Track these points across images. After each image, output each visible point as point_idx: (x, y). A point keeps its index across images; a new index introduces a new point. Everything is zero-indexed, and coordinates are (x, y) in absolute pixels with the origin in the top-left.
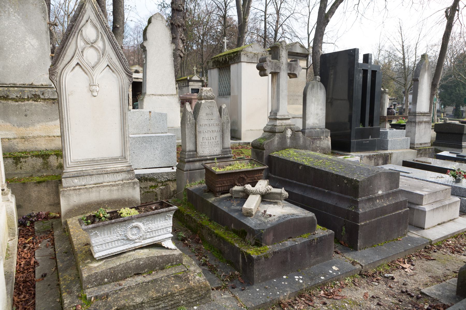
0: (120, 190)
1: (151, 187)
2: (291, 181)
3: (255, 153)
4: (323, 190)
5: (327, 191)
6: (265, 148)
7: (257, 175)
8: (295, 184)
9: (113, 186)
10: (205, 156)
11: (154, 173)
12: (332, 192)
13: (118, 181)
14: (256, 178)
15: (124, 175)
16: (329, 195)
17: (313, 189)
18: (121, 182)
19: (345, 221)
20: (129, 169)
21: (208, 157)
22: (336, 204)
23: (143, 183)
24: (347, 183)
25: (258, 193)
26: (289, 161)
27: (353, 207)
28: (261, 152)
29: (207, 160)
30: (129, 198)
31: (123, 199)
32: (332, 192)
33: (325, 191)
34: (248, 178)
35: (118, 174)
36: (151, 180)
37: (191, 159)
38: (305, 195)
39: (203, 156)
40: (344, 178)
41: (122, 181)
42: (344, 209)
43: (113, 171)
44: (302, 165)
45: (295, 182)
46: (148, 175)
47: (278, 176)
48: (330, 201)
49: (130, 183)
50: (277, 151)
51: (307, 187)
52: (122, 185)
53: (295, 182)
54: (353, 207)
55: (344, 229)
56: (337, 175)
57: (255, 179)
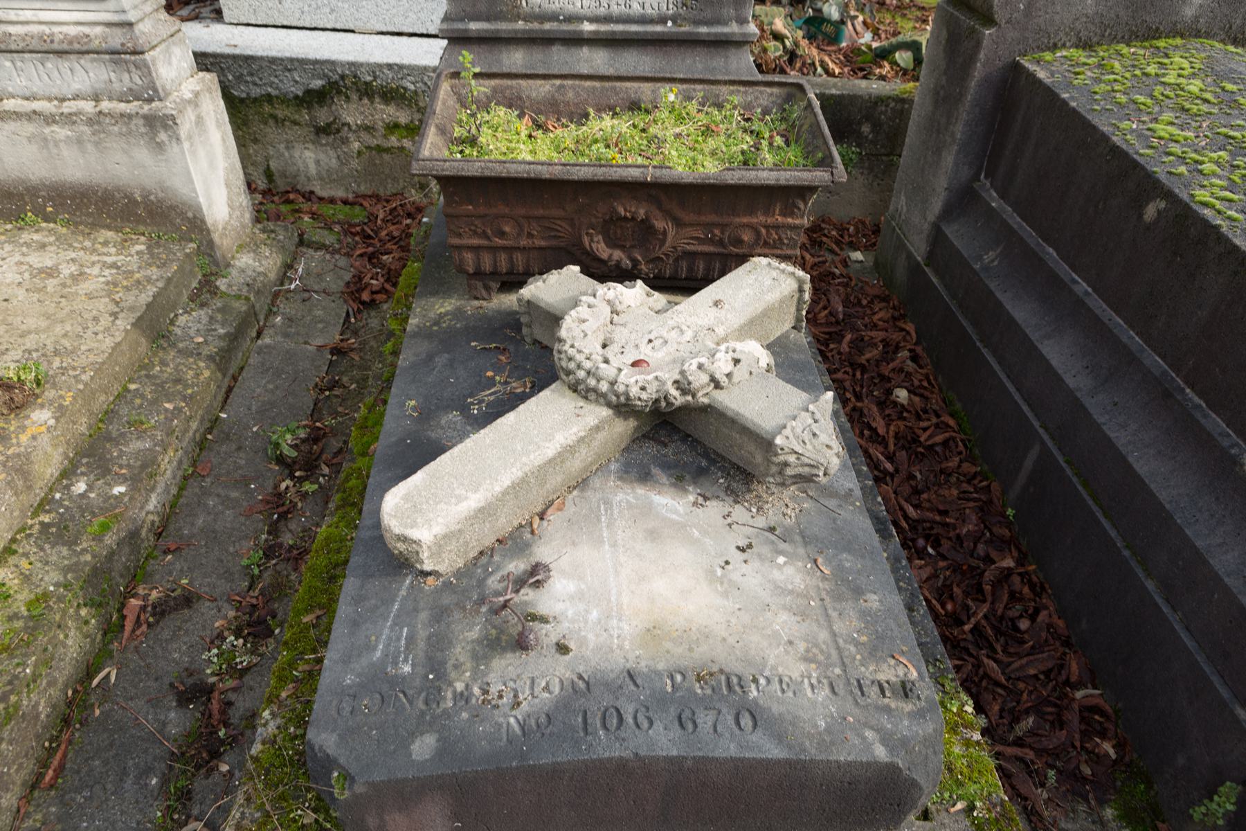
0: (90, 147)
1: (393, 127)
3: (944, 34)
6: (1000, 15)
7: (759, 219)
8: (1080, 303)
9: (50, 119)
10: (570, 19)
11: (401, 67)
13: (76, 97)
14: (747, 237)
15: (83, 77)
18: (88, 107)
20: (117, 39)
21: (588, 27)
23: (353, 106)
25: (604, 395)
26: (1105, 138)
28: (973, 31)
29: (577, 41)
30: (146, 195)
31: (118, 190)
34: (679, 223)
35: (64, 64)
36: (392, 95)
37: (474, 26)
38: (1097, 406)
39: (554, 17)
41: (97, 99)
43: (35, 44)
44: (1169, 195)
45: (1082, 287)
46: (375, 69)
47: (1016, 206)
49: (130, 117)
50: (1086, 45)
51: (1130, 358)
52: (90, 122)
53: (1082, 287)
57: (738, 242)
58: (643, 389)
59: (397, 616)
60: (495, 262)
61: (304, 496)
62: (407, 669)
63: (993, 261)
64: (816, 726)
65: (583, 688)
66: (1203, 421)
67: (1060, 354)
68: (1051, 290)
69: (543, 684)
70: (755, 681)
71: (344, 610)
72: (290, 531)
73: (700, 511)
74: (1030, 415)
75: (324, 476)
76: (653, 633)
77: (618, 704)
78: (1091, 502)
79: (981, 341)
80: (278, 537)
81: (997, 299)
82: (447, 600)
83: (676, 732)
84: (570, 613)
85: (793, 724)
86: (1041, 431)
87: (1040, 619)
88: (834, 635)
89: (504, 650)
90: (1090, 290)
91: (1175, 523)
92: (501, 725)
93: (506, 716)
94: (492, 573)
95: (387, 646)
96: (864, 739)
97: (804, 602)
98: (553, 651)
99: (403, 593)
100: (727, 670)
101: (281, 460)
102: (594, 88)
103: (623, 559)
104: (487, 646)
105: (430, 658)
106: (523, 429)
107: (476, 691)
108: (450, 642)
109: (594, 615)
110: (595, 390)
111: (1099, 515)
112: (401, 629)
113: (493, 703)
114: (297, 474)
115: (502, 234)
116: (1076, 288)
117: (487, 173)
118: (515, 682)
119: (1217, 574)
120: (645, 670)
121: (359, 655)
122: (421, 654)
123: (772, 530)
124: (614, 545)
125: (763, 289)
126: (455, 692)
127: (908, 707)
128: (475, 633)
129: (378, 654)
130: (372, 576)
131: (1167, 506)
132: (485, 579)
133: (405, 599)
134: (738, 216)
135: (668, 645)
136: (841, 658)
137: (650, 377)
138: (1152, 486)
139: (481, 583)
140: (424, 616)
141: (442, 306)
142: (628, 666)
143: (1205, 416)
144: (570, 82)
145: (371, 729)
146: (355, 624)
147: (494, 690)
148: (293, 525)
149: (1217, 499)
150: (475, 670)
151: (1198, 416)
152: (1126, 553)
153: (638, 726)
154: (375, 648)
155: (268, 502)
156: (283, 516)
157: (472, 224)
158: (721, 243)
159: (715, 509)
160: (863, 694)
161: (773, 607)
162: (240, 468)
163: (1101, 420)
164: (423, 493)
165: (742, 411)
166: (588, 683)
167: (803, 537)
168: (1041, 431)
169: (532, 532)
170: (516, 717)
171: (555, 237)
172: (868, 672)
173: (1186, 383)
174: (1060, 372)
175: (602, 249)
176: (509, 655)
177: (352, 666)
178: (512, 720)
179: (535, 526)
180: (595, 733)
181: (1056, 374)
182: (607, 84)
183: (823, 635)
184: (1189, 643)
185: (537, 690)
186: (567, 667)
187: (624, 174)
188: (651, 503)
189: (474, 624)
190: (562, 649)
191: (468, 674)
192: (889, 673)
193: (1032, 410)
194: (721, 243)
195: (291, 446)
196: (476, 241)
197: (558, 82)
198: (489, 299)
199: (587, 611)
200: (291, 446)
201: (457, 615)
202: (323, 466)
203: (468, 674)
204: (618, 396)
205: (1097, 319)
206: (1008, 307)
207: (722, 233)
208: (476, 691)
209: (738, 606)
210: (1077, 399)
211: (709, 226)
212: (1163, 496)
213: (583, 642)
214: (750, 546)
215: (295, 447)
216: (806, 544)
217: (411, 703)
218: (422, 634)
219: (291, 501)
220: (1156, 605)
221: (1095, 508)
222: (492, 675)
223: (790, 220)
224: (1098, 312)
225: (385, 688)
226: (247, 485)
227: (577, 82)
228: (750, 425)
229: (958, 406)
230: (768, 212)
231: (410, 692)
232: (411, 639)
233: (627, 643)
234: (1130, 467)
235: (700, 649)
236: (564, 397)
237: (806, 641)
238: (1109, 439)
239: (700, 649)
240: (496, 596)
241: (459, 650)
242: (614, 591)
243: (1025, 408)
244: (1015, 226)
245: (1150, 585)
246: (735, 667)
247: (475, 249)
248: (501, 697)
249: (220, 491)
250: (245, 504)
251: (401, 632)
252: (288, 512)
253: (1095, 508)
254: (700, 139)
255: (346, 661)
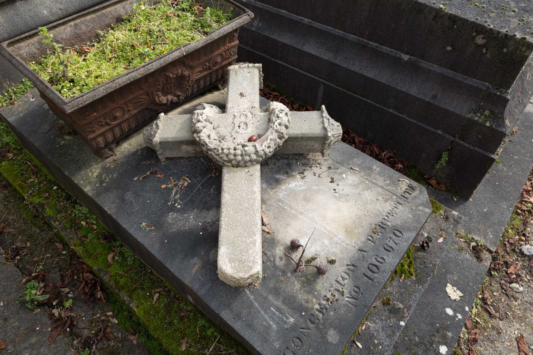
2: (294, 16)
4: (394, 52)
5: (406, 57)
8: (309, 28)
12: (424, 64)
16: (413, 69)
17: (365, 47)
19: (452, 142)
22: (434, 97)
24: (484, 46)
25: (255, 160)
27: (487, 113)
32: (424, 64)
33: (400, 59)
38: (339, 61)
40: (480, 29)
42: (459, 116)
48: (414, 88)
51: (344, 40)
53: (306, 20)
54: (487, 113)
55: (445, 157)
56: (454, 19)
57: (217, 63)
58: (269, 147)
59: (262, 307)
60: (114, 134)
61: (71, 309)
62: (292, 320)
63: (258, 24)
64: (410, 218)
65: (353, 267)
66: (382, 50)
67: (312, 48)
68: (293, 27)
69: (341, 279)
70: (385, 219)
71: (237, 326)
72: (84, 328)
73: (306, 179)
74: (312, 76)
75: (69, 293)
76: (348, 232)
77: (369, 262)
78: (355, 95)
79: (273, 58)
80: (82, 336)
81: (273, 39)
82: (271, 284)
83: (391, 255)
84: (318, 249)
85: (406, 223)
86: (321, 80)
87: (356, 141)
88: (382, 187)
89: (315, 281)
90: (310, 21)
91: (392, 87)
92: (346, 304)
93: (343, 300)
94: (274, 260)
95: (273, 320)
96: (421, 210)
97: (364, 184)
98: (330, 265)
99: (252, 297)
100: (377, 223)
101: (41, 305)
102: (93, 18)
103: (310, 216)
104: (307, 285)
105: (294, 309)
106: (238, 197)
107: (324, 302)
108: (293, 296)
109: (327, 242)
110: (251, 161)
111: (361, 98)
112: (270, 309)
113: (335, 300)
114: (54, 303)
115: (115, 118)
116: (303, 22)
117: (109, 91)
118: (332, 287)
119: (415, 96)
120: (362, 245)
121: (268, 334)
122: (289, 310)
123: (330, 168)
124: (302, 214)
125: (245, 80)
126: (317, 310)
127: (417, 192)
128: (297, 286)
129: (274, 326)
130: (230, 304)
131: (387, 83)
132: (275, 265)
133: (255, 299)
134: (214, 52)
135: (356, 231)
136: (391, 192)
137: (269, 141)
138: (378, 79)
139: (275, 266)
140: (271, 297)
141: (93, 173)
142: (357, 247)
143: (382, 48)
144: (79, 21)
145: (309, 351)
146: (250, 326)
147: (329, 296)
148: (81, 325)
149: (399, 73)
150: (315, 296)
151: (379, 49)
152: (378, 105)
153: (381, 263)
154: (270, 326)
155: (56, 328)
156: (71, 326)
157: (99, 122)
158: (210, 68)
159: (308, 174)
160: (407, 198)
161: (361, 193)
162: (19, 327)
163: (345, 66)
164: (236, 253)
165: (303, 132)
166: (353, 265)
167: (339, 163)
168: (321, 80)
169: (268, 233)
170: (347, 297)
171: (141, 105)
172: (400, 192)
173: (368, 40)
174: (319, 55)
175: (164, 99)
176: (319, 281)
177: (271, 340)
178: (346, 299)
179: (267, 230)
180: (375, 278)
181: (317, 57)
182: (98, 14)
183: (380, 190)
184: (414, 121)
185: (342, 282)
186: (340, 266)
187: (173, 57)
188: (291, 189)
189: (293, 283)
190: (332, 262)
191: (314, 300)
192: (404, 187)
193: (312, 74)
194: (210, 68)
195: (42, 294)
196: (103, 130)
197: (72, 23)
198: (114, 154)
199: (322, 243)
200: (42, 294)
201: (283, 286)
202: (63, 290)
203: (314, 300)
204: (262, 157)
205: (321, 31)
206: (280, 40)
207: (209, 63)
208: (324, 302)
209: (354, 201)
210: (331, 63)
211: (203, 64)
212: (383, 81)
213: (335, 254)
214: (332, 179)
215: (44, 293)
216: (342, 165)
217: (309, 329)
218: (279, 303)
219: (68, 317)
220: (397, 116)
221: (358, 96)
222: (322, 292)
223: (233, 44)
224: (319, 27)
225: (294, 334)
226: (34, 330)
227: (82, 19)
228: (311, 135)
229: (274, 86)
230: (224, 45)
231: (304, 326)
232: (278, 309)
233: (347, 241)
234: (366, 77)
235: (364, 224)
236: (236, 172)
237: (379, 195)
238: (353, 71)
239: (364, 224)
240: (289, 265)
241: (300, 296)
242: (322, 229)
243: (309, 75)
244: (261, 7)
245: (391, 111)
246: (378, 220)
247: (103, 134)
248: (334, 296)
249: (25, 345)
250: (45, 339)
251: (272, 311)
252: (72, 322)
253: (358, 96)
254: (168, 23)
255: (265, 341)
